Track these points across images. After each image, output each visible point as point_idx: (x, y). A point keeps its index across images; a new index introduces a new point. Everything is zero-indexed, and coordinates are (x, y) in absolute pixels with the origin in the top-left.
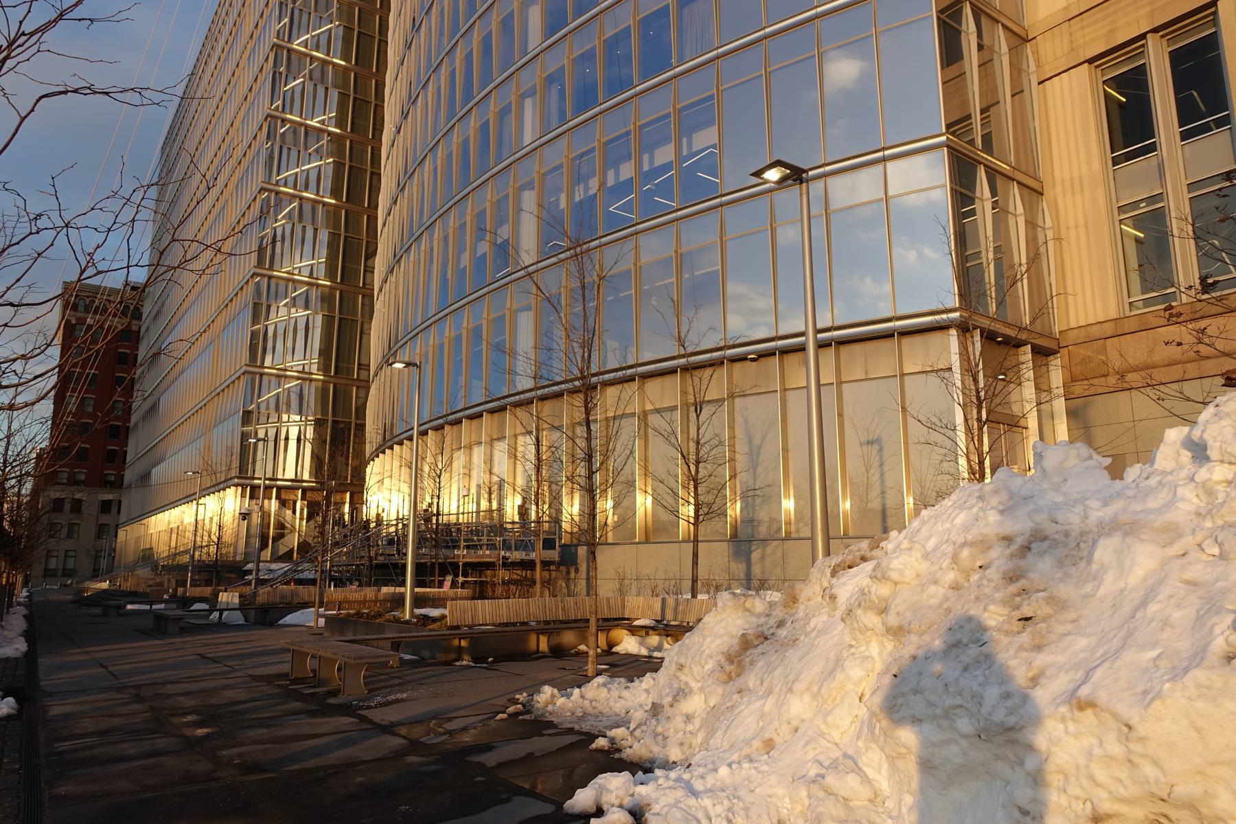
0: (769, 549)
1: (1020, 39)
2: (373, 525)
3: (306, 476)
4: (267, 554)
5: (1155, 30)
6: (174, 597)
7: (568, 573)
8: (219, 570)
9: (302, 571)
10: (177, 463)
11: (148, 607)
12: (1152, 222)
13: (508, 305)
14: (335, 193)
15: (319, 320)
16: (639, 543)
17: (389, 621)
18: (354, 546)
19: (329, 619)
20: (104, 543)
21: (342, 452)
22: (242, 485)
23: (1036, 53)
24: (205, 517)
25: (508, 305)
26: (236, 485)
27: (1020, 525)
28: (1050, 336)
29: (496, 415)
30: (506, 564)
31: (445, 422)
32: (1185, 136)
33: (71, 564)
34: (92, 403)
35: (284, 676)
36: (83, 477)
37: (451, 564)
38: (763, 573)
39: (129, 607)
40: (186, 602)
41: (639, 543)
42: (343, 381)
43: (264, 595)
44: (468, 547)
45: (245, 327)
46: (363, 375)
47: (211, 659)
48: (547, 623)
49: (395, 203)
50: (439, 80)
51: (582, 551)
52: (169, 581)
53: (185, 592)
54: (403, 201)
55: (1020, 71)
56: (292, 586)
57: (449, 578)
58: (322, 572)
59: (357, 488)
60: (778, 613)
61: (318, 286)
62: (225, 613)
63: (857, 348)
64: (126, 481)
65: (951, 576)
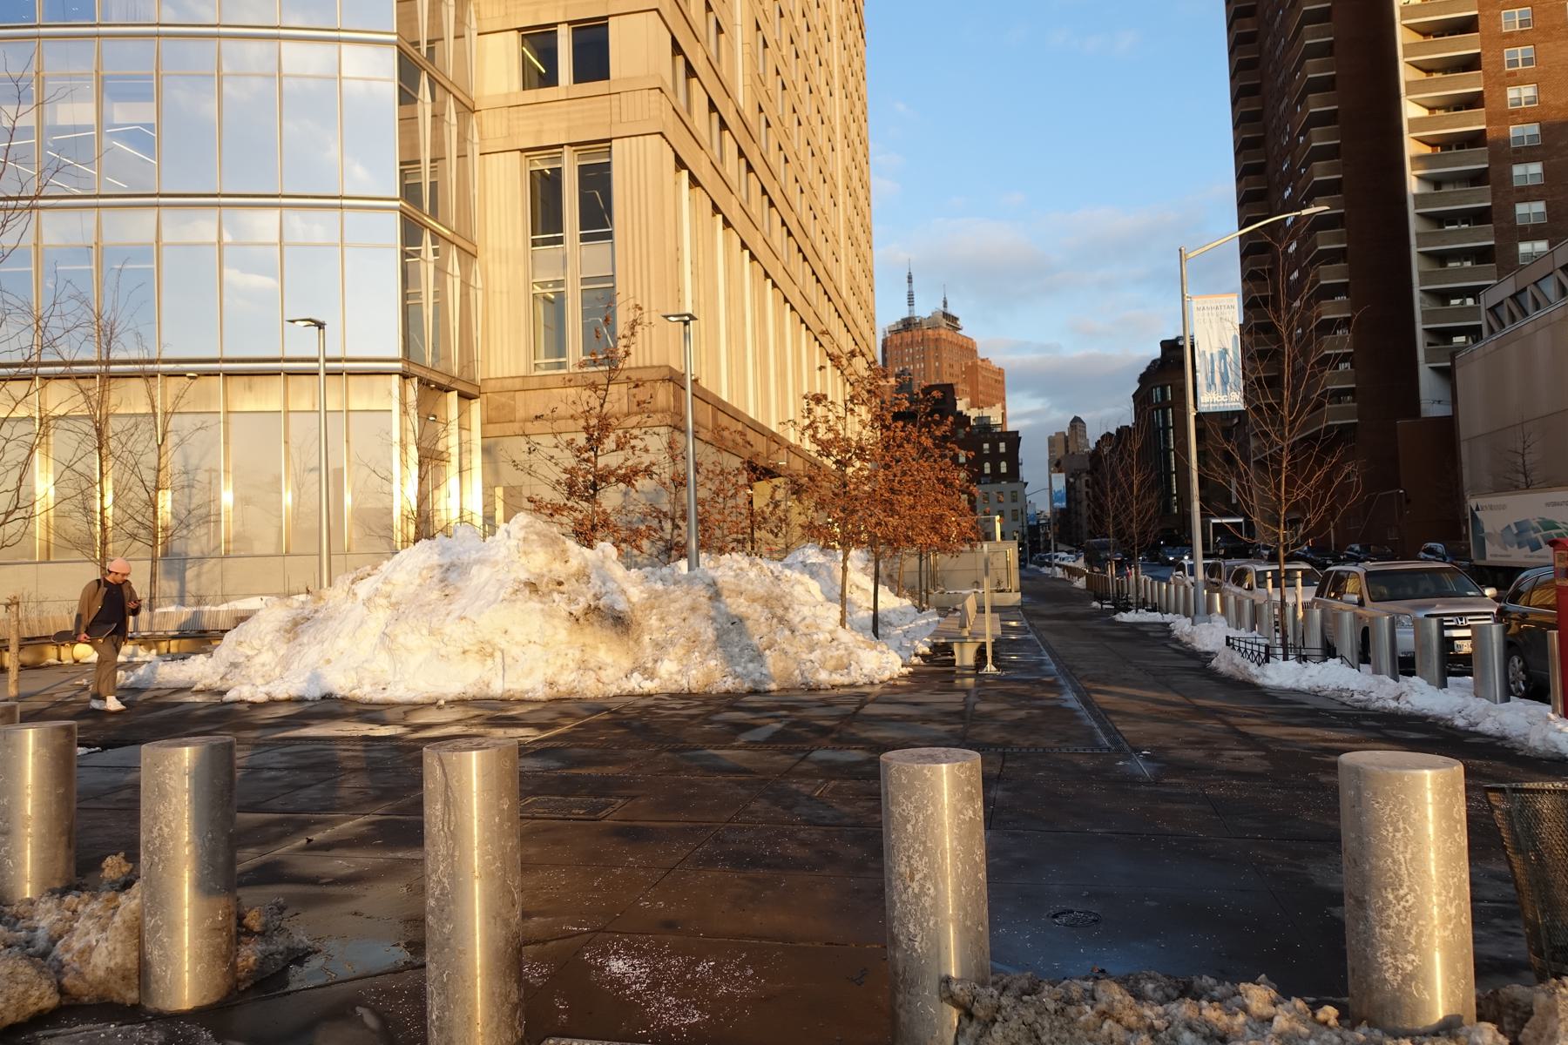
0: (206, 567)
1: (467, 109)
5: (571, 145)
12: (555, 305)
23: (480, 125)
27: (446, 561)
28: (471, 383)
32: (584, 238)
55: (465, 140)
60: (310, 607)
65: (418, 581)
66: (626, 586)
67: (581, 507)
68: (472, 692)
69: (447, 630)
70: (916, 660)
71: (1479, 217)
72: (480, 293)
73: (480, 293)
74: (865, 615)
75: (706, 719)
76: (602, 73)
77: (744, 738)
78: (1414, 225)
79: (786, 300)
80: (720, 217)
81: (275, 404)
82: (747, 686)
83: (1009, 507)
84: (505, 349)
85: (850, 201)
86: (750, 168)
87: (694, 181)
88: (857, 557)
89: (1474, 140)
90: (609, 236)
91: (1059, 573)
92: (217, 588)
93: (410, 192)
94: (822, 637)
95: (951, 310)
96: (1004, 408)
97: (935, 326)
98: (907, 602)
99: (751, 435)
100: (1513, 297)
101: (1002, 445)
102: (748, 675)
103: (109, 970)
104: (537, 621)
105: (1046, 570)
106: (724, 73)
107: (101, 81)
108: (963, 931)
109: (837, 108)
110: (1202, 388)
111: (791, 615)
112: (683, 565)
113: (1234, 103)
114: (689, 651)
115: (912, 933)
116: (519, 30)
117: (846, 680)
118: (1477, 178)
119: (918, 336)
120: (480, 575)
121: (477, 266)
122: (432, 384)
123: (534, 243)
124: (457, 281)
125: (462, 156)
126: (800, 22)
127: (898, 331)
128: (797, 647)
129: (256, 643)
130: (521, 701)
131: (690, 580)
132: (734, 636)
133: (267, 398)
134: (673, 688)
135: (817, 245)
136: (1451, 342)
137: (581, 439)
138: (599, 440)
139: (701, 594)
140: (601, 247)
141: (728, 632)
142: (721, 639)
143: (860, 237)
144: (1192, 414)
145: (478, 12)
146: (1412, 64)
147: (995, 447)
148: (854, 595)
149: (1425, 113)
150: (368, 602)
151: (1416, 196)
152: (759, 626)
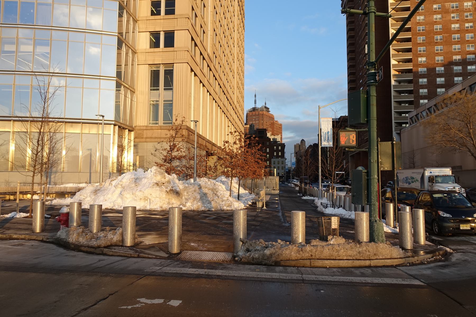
0: (57, 175)
1: (134, 52)
23: (138, 57)
27: (136, 177)
28: (132, 127)
32: (165, 89)
66: (179, 185)
67: (168, 164)
68: (142, 208)
69: (137, 194)
70: (247, 206)
71: (410, 92)
72: (135, 103)
73: (135, 103)
74: (236, 194)
75: (199, 215)
76: (172, 46)
77: (207, 219)
78: (393, 93)
79: (219, 106)
80: (202, 84)
81: (78, 131)
82: (207, 209)
83: (281, 165)
84: (142, 118)
85: (238, 77)
86: (210, 70)
87: (195, 75)
88: (235, 180)
89: (410, 71)
90: (172, 89)
91: (293, 185)
92: (60, 181)
93: (119, 74)
94: (225, 199)
95: (267, 106)
96: (281, 136)
97: (262, 109)
98: (247, 192)
99: (207, 144)
100: (416, 115)
101: (280, 147)
102: (207, 207)
103: (117, 240)
104: (158, 192)
105: (289, 184)
106: (205, 44)
107: (35, 40)
108: (243, 232)
109: (235, 51)
110: (323, 141)
111: (218, 193)
112: (192, 180)
113: (348, 55)
114: (194, 201)
115: (236, 232)
116: (150, 32)
117: (230, 209)
118: (410, 82)
119: (257, 113)
120: (144, 181)
121: (135, 95)
122: (122, 127)
123: (151, 90)
124: (130, 100)
125: (132, 65)
126: (226, 27)
127: (251, 111)
128: (219, 201)
129: (85, 195)
130: (155, 211)
131: (194, 184)
132: (204, 198)
133: (76, 129)
134: (190, 209)
135: (228, 90)
136: (402, 126)
137: (169, 148)
138: (173, 149)
139: (197, 187)
140: (169, 92)
141: (203, 196)
142: (201, 198)
143: (241, 86)
144: (320, 147)
145: (139, 26)
146: (394, 49)
147: (278, 148)
148: (234, 189)
149: (397, 63)
150: (115, 187)
151: (394, 85)
152: (210, 195)
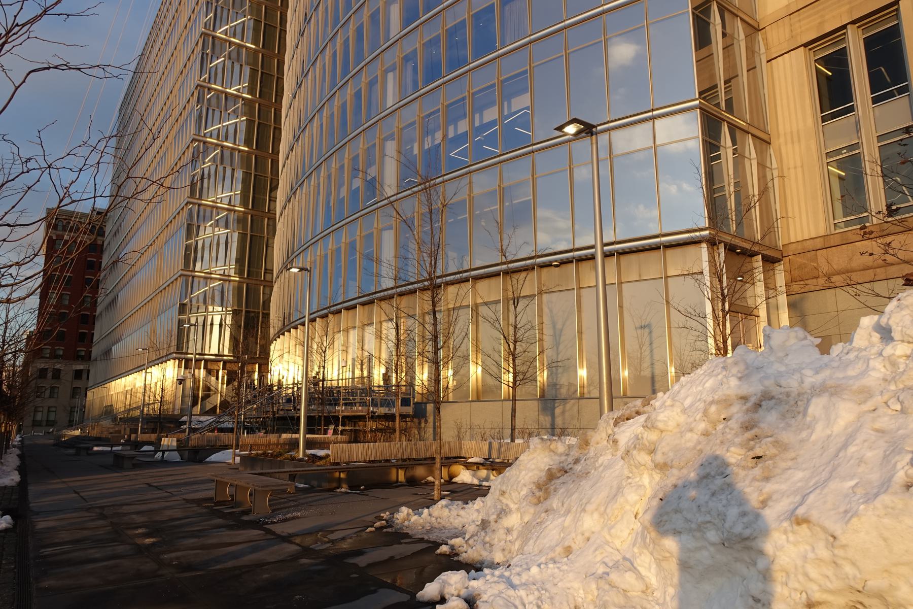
0: (568, 406)
1: (754, 29)
2: (275, 388)
3: (226, 352)
4: (197, 409)
5: (853, 22)
6: (128, 441)
7: (420, 423)
8: (162, 421)
9: (223, 422)
10: (131, 342)
11: (109, 449)
12: (851, 164)
13: (375, 226)
14: (248, 142)
15: (236, 236)
16: (472, 401)
17: (288, 459)
18: (261, 403)
19: (243, 458)
20: (77, 401)
21: (252, 334)
22: (179, 359)
23: (765, 39)
24: (151, 382)
25: (375, 226)
26: (175, 359)
27: (754, 388)
28: (775, 249)
29: (366, 307)
30: (374, 417)
31: (329, 312)
32: (875, 101)
33: (52, 417)
34: (68, 297)
35: (210, 499)
36: (61, 353)
37: (333, 417)
38: (564, 423)
39: (95, 448)
40: (137, 445)
41: (472, 401)
42: (254, 282)
43: (195, 439)
44: (346, 404)
45: (181, 242)
46: (268, 277)
47: (156, 487)
48: (404, 460)
49: (292, 150)
50: (324, 59)
51: (430, 407)
52: (125, 430)
53: (137, 437)
54: (298, 149)
55: (753, 52)
56: (216, 433)
57: (332, 427)
58: (238, 423)
59: (264, 360)
60: (575, 453)
61: (235, 211)
62: (166, 453)
63: (633, 257)
64: (93, 355)
65: (702, 426)
